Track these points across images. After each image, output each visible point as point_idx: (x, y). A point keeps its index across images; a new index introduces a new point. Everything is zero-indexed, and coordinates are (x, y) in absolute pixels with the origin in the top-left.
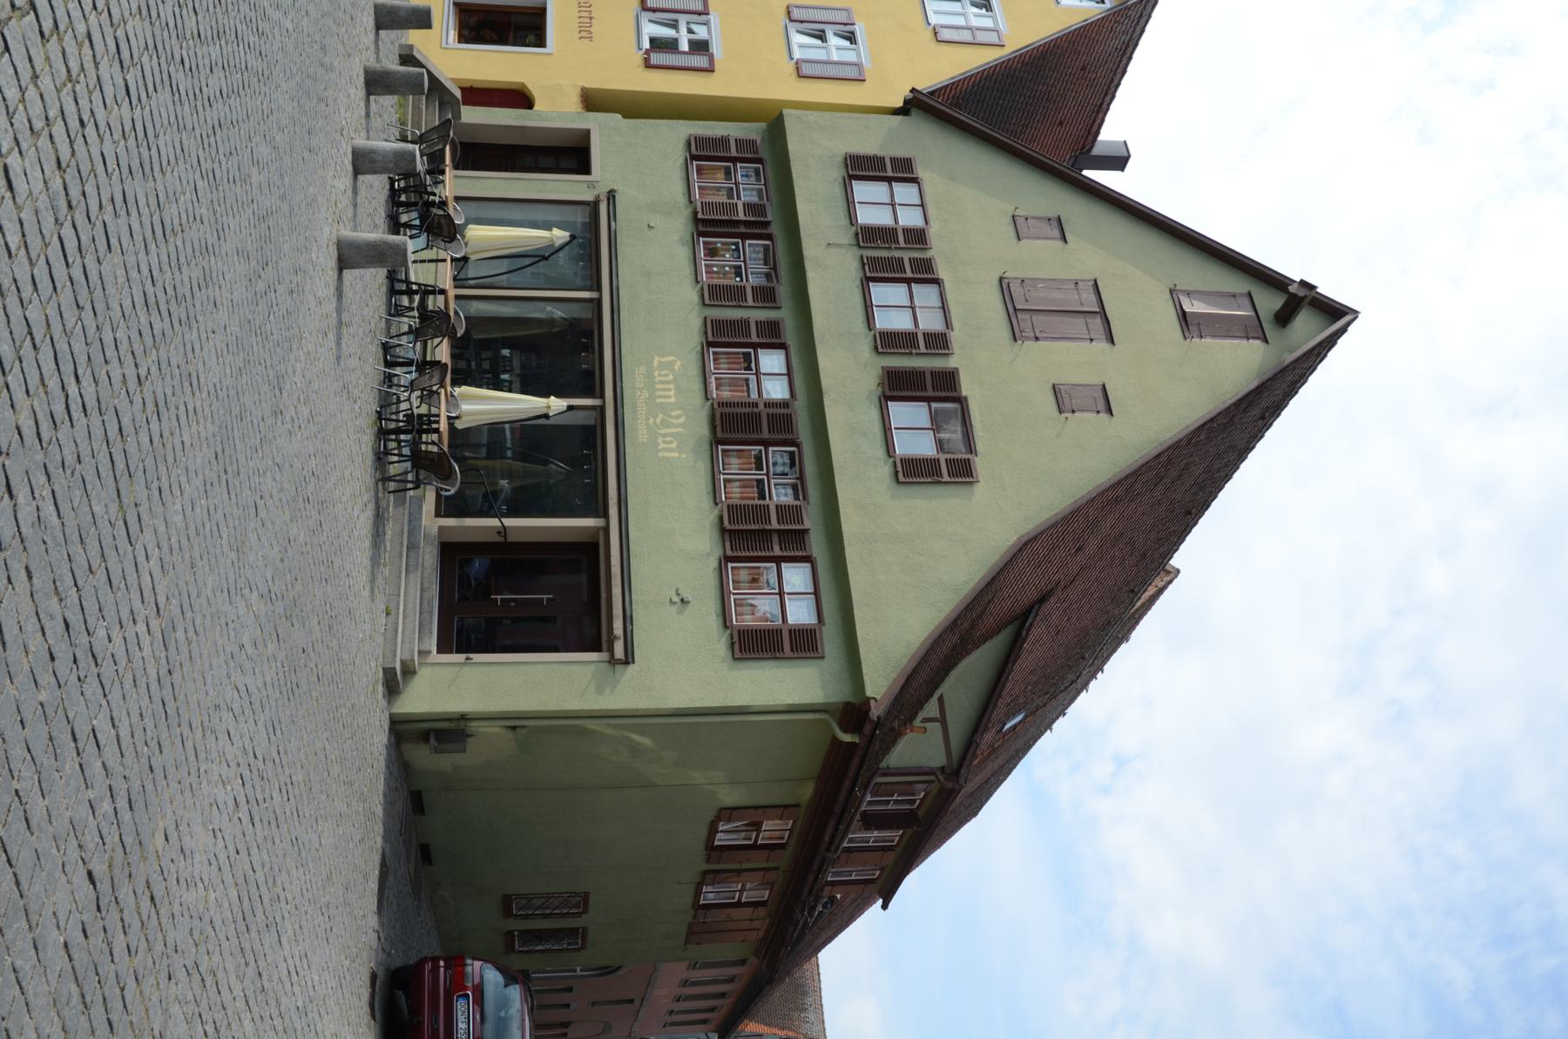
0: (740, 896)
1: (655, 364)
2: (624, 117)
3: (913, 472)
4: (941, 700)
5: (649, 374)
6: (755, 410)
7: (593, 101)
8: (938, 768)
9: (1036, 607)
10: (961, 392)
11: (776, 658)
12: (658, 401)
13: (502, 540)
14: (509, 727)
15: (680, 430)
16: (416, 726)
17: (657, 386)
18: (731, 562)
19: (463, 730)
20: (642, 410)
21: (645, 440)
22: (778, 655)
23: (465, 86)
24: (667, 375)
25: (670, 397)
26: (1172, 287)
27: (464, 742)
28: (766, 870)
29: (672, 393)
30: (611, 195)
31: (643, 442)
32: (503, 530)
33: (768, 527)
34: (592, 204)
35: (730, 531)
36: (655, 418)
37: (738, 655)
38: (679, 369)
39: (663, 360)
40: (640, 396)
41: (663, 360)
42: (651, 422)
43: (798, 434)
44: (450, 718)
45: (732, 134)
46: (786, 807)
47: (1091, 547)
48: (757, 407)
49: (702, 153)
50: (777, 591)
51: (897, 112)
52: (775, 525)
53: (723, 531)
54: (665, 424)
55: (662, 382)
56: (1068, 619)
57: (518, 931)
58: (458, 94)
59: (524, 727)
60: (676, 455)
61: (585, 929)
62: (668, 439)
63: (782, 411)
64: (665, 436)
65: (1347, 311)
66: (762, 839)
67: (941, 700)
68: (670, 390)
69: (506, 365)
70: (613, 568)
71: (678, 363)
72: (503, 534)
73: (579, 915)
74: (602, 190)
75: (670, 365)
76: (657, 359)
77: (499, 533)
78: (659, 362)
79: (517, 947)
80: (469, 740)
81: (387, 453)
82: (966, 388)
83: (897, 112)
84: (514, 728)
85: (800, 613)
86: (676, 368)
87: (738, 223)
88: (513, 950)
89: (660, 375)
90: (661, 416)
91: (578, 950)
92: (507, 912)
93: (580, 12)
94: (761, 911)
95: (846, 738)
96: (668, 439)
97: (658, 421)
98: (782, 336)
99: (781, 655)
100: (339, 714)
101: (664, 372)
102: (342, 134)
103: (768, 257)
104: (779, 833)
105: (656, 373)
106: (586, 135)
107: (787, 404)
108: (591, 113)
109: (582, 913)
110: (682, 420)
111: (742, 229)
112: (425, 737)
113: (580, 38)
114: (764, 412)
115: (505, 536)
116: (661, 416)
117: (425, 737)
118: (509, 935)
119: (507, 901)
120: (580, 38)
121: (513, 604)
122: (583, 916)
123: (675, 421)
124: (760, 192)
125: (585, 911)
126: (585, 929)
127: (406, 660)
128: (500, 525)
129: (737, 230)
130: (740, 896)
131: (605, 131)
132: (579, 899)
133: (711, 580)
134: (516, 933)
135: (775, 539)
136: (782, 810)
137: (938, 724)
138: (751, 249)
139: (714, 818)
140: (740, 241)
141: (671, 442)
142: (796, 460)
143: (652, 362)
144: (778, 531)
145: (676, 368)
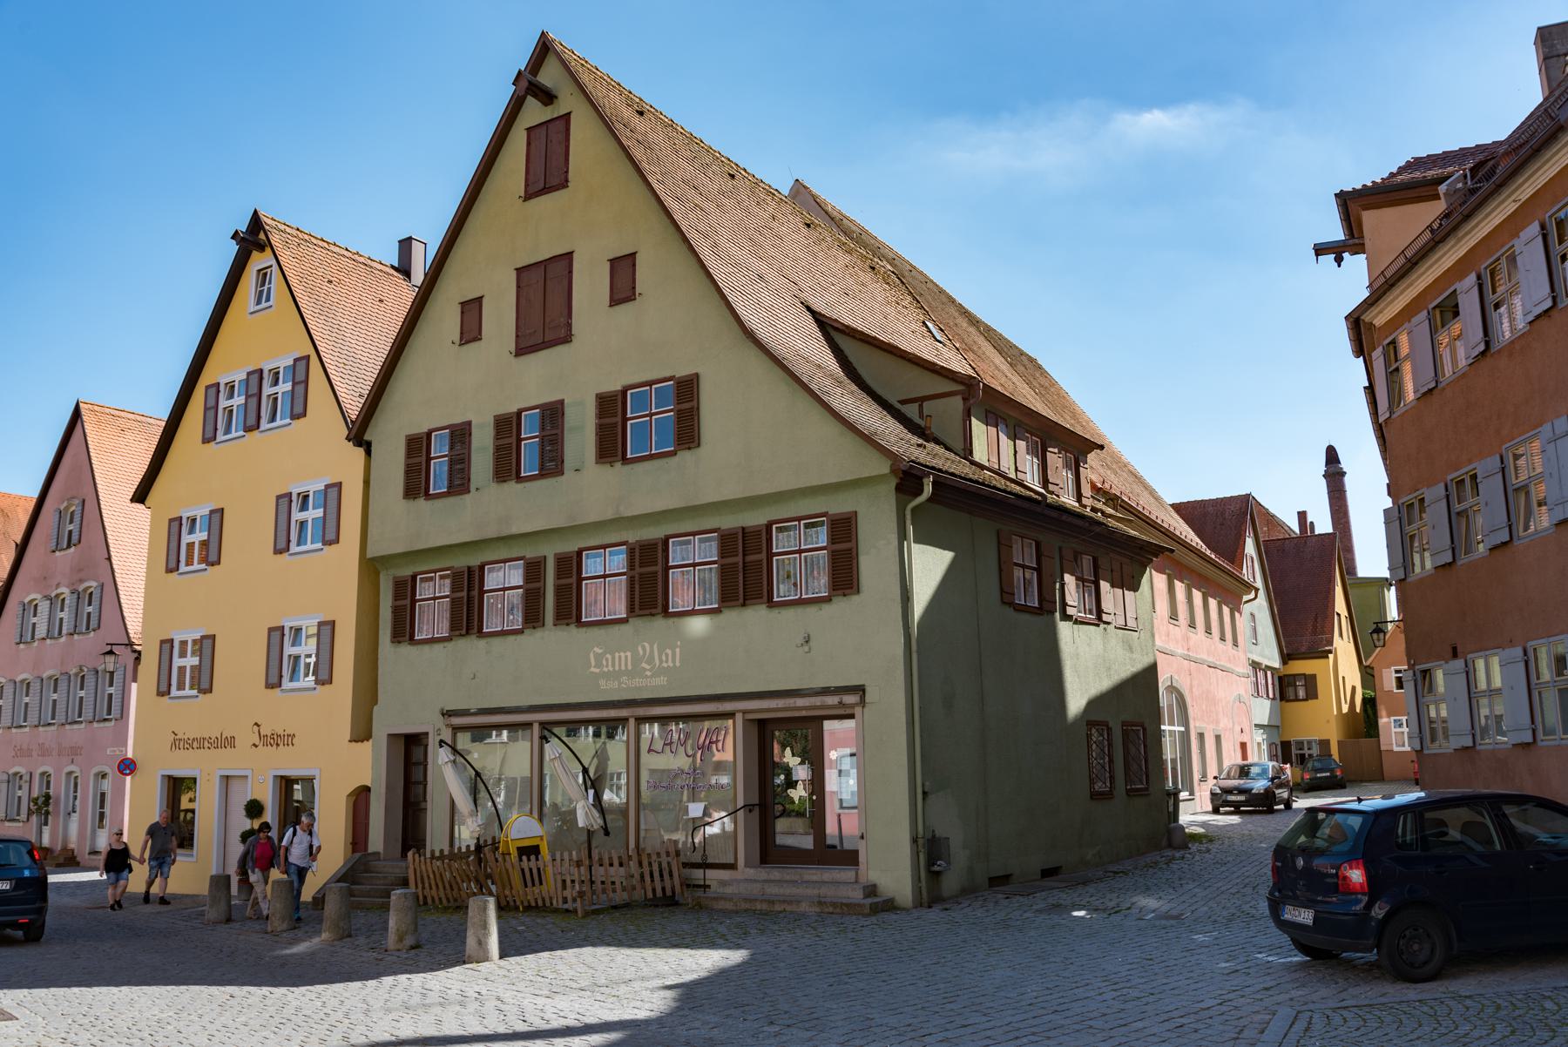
0: (1088, 581)
1: (597, 670)
2: (376, 703)
3: (687, 433)
4: (903, 402)
5: (607, 676)
6: (637, 578)
7: (362, 732)
8: (964, 404)
9: (817, 316)
10: (618, 391)
11: (544, 594)
12: (630, 668)
13: (757, 809)
14: (924, 799)
15: (655, 646)
16: (924, 883)
17: (617, 668)
18: (773, 598)
19: (928, 840)
20: (638, 682)
21: (666, 679)
22: (542, 592)
23: (351, 850)
24: (607, 660)
25: (626, 657)
26: (521, 199)
27: (939, 839)
28: (1061, 558)
29: (622, 654)
30: (447, 714)
31: (667, 681)
32: (748, 808)
33: (741, 564)
34: (455, 731)
35: (745, 600)
36: (645, 670)
37: (541, 623)
38: (601, 648)
39: (593, 663)
40: (626, 684)
41: (593, 663)
42: (648, 673)
43: (659, 539)
44: (915, 855)
45: (390, 604)
46: (999, 543)
47: (762, 267)
48: (634, 577)
49: (404, 630)
50: (797, 555)
51: (368, 453)
52: (739, 559)
53: (744, 605)
54: (650, 661)
55: (613, 665)
56: (833, 285)
57: (1126, 785)
58: (357, 855)
59: (923, 785)
60: (678, 650)
61: (1124, 724)
62: (664, 658)
63: (637, 554)
64: (661, 661)
65: (542, 40)
66: (1032, 562)
67: (903, 402)
68: (620, 657)
69: (190, 828)
70: (771, 707)
71: (596, 649)
72: (751, 807)
73: (1109, 729)
74: (440, 722)
75: (598, 658)
76: (593, 669)
77: (750, 811)
78: (595, 667)
79: (1143, 786)
80: (937, 836)
81: (835, 908)
82: (615, 386)
83: (368, 453)
84: (925, 793)
85: (515, 576)
86: (600, 651)
87: (469, 599)
88: (1147, 789)
89: (607, 666)
90: (644, 665)
91: (1144, 729)
92: (1107, 796)
93: (288, 745)
94: (1103, 562)
95: (928, 489)
96: (664, 658)
97: (648, 667)
98: (759, 529)
99: (542, 589)
100: (1020, 951)
101: (604, 663)
102: (381, 960)
103: (784, 524)
104: (1025, 549)
105: (605, 669)
106: (393, 737)
107: (631, 549)
108: (373, 734)
109: (1107, 726)
110: (647, 645)
111: (475, 593)
112: (935, 876)
113: (293, 745)
114: (638, 570)
115: (754, 805)
116: (644, 665)
117: (935, 876)
118: (1130, 793)
119: (1095, 796)
120: (293, 745)
121: (814, 798)
122: (1110, 725)
123: (648, 654)
124: (442, 577)
125: (1106, 724)
126: (1124, 724)
127: (864, 894)
128: (742, 810)
129: (476, 597)
130: (1088, 581)
131: (391, 719)
132: (1094, 731)
133: (789, 614)
134: (1129, 787)
135: (750, 558)
136: (1003, 546)
137: (925, 404)
138: (423, 593)
139: (1012, 609)
140: (775, 558)
141: (667, 655)
142: (784, 524)
143: (596, 673)
144: (744, 555)
145: (600, 651)
